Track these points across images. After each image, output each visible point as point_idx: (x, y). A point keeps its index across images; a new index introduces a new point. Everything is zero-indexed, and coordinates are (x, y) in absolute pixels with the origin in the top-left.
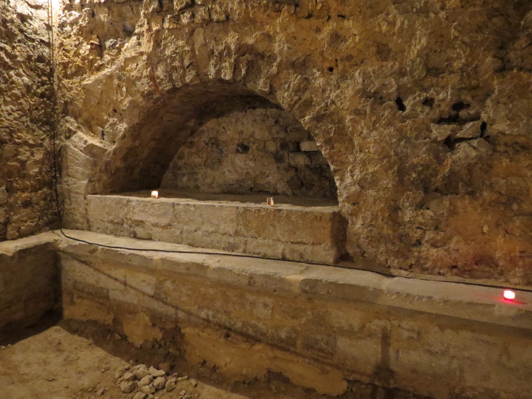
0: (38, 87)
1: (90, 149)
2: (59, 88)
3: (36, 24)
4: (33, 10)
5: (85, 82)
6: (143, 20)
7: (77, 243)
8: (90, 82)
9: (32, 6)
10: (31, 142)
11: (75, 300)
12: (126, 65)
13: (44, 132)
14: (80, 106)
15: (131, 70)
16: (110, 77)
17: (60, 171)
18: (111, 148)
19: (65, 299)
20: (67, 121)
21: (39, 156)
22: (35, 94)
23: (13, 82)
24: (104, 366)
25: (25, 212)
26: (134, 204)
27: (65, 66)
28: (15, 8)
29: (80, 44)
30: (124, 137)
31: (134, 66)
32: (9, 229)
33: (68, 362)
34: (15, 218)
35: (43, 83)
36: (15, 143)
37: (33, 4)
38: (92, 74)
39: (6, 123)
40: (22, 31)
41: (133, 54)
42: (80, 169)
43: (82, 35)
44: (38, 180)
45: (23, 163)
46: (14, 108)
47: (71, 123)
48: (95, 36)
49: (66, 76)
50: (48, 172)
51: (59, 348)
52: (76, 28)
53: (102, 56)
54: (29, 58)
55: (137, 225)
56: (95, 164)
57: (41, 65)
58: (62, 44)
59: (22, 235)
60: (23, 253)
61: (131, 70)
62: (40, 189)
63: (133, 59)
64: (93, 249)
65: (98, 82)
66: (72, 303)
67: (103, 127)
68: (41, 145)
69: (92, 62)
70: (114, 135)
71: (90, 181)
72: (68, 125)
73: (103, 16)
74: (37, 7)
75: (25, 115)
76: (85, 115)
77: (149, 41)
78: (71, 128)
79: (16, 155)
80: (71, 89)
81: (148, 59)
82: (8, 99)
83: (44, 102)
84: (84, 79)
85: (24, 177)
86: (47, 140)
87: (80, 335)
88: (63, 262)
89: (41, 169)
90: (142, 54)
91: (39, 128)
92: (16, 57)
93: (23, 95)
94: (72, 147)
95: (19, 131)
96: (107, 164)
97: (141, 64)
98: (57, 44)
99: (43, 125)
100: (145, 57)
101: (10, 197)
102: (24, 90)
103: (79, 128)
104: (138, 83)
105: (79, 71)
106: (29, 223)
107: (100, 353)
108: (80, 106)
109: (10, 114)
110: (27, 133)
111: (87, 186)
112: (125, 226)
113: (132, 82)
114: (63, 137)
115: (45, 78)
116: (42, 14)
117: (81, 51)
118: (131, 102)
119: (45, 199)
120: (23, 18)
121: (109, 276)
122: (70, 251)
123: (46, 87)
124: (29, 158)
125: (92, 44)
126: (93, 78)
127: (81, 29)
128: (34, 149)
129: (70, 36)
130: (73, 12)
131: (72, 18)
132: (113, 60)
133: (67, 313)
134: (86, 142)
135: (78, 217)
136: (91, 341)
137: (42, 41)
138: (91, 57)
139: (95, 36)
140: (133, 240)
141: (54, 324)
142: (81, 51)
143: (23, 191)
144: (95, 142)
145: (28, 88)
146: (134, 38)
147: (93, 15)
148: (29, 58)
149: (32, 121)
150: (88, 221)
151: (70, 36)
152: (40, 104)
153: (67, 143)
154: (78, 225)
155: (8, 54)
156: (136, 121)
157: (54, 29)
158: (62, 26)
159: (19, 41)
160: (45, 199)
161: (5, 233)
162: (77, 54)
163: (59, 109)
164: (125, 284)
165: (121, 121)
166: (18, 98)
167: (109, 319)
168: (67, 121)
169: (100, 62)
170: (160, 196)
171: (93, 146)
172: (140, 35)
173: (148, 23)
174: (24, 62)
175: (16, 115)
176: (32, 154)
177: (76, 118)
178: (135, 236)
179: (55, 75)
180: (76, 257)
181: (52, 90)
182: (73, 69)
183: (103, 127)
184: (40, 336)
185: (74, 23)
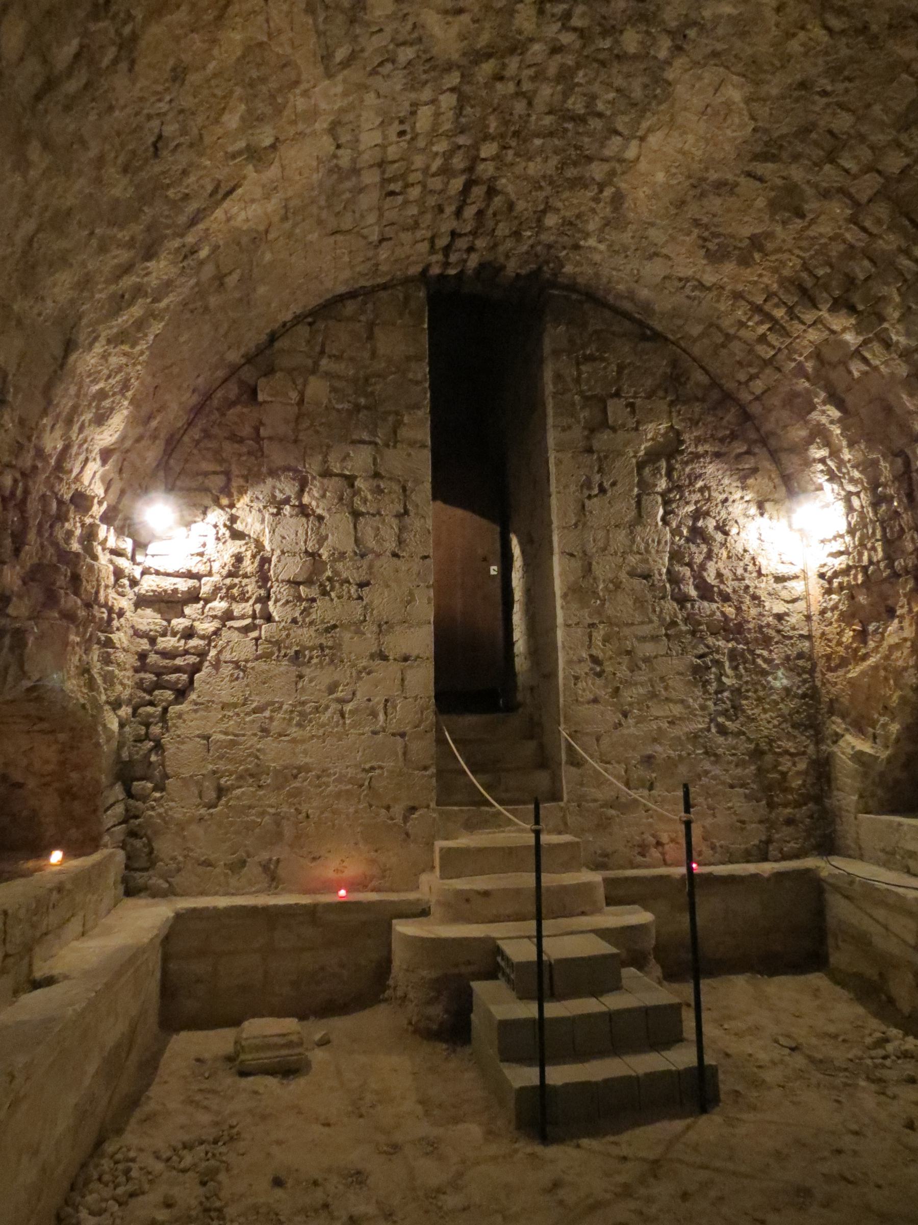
0: (799, 687)
1: (858, 757)
2: (824, 684)
3: (793, 620)
4: (790, 606)
5: (850, 675)
6: (903, 600)
7: (837, 872)
8: (855, 675)
9: (788, 602)
10: (792, 750)
11: (840, 944)
12: (891, 653)
13: (808, 737)
14: (847, 703)
15: (897, 660)
16: (875, 668)
17: (829, 781)
18: (884, 754)
19: (831, 941)
20: (834, 723)
21: (802, 766)
22: (796, 696)
23: (771, 688)
24: (860, 1023)
25: (787, 831)
26: (905, 828)
27: (828, 657)
28: (770, 610)
29: (843, 631)
30: (898, 740)
31: (899, 654)
32: (771, 848)
33: (821, 1008)
34: (777, 836)
35: (805, 681)
36: (775, 753)
37: (789, 599)
38: (857, 664)
39: (766, 732)
40: (779, 631)
41: (897, 641)
42: (849, 781)
43: (843, 621)
44: (801, 794)
45: (784, 774)
46: (773, 715)
47: (837, 724)
48: (857, 621)
49: (830, 669)
50: (813, 785)
51: (816, 993)
52: (837, 613)
53: (865, 643)
54: (788, 658)
55: (910, 857)
56: (865, 775)
57: (801, 663)
58: (823, 634)
59: (785, 857)
60: (780, 876)
61: (897, 660)
62: (805, 804)
63: (897, 646)
64: (851, 879)
65: (863, 674)
66: (838, 947)
67: (874, 728)
68: (804, 753)
69: (856, 650)
70: (887, 738)
71: (861, 796)
72: (834, 727)
73: (862, 599)
74: (794, 601)
75: (785, 721)
76: (854, 714)
77: (911, 625)
78: (838, 730)
79: (775, 767)
80: (836, 683)
81: (912, 646)
82: (767, 706)
83: (806, 704)
84: (849, 671)
85: (786, 790)
86: (812, 747)
87: (843, 987)
88: (827, 895)
89: (805, 781)
90: (905, 640)
91: (802, 733)
92: (773, 660)
93: (783, 700)
94: (839, 754)
95: (779, 739)
96: (882, 774)
97: (906, 651)
98: (817, 633)
99: (806, 730)
100: (909, 644)
101: (770, 812)
102: (783, 694)
103: (847, 730)
104: (906, 674)
105: (844, 663)
106: (792, 844)
107: (860, 1010)
108: (847, 703)
109: (769, 722)
110: (788, 740)
111: (858, 802)
112: (898, 857)
113: (898, 673)
114: (829, 742)
115: (806, 676)
116: (801, 606)
117: (844, 639)
118: (902, 698)
119: (811, 817)
120: (780, 617)
121: (871, 916)
122: (831, 881)
123: (807, 685)
124: (790, 769)
125: (854, 630)
126: (858, 669)
127: (842, 614)
128: (796, 759)
129: (831, 624)
130: (834, 596)
131: (832, 603)
132: (877, 647)
133: (832, 960)
134: (853, 747)
135: (850, 842)
136: (852, 996)
137: (801, 636)
138: (855, 645)
139: (857, 621)
140: (906, 876)
141: (818, 970)
142: (844, 639)
143: (785, 805)
144: (865, 747)
145: (787, 690)
146: (896, 621)
147: (852, 597)
148: (788, 658)
149: (793, 726)
150: (860, 848)
151: (831, 624)
152: (801, 707)
153: (835, 749)
154: (851, 852)
155: (765, 660)
156: (910, 721)
157: (814, 618)
158: (823, 612)
159: (777, 643)
160: (811, 817)
161: (767, 853)
162: (839, 643)
163: (824, 708)
164: (887, 928)
165: (893, 720)
166: (777, 703)
167: (871, 972)
168: (834, 723)
169: (863, 651)
170: (66, 856)
171: (862, 753)
172: (901, 618)
173: (909, 604)
174: (782, 664)
175: (776, 722)
176: (794, 764)
177: (843, 717)
178: (908, 872)
179: (818, 669)
180: (837, 889)
181: (814, 688)
182: (837, 661)
183: (874, 728)
184: (802, 978)
185: (834, 608)
